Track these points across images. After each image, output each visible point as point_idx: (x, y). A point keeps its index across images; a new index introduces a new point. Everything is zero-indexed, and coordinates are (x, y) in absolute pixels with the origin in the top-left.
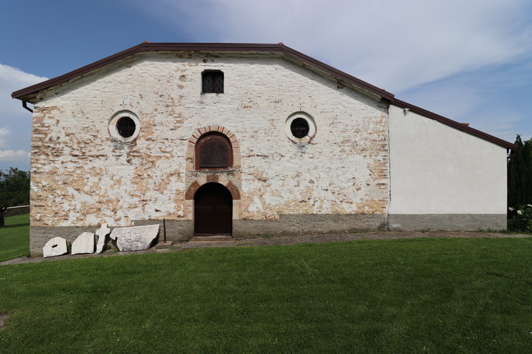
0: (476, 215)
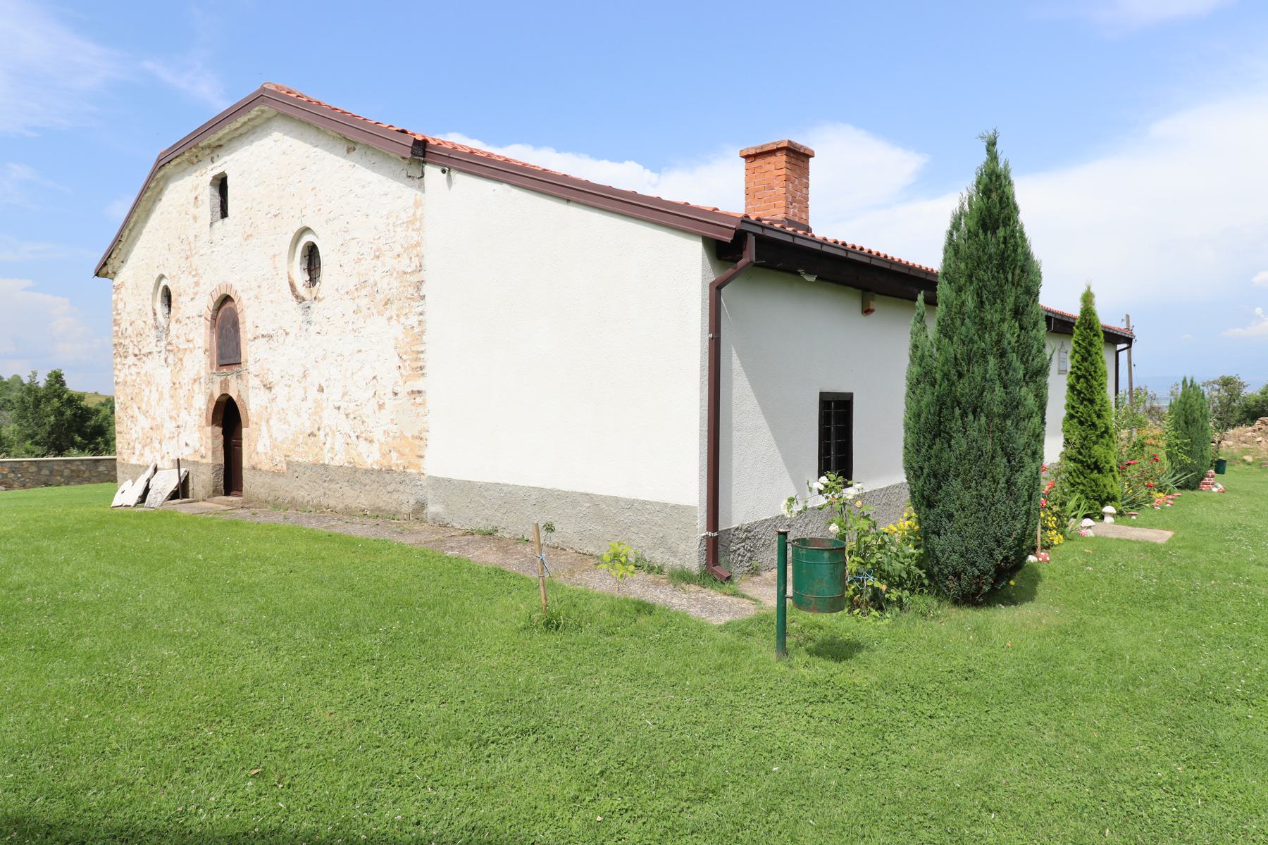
0: (604, 499)
